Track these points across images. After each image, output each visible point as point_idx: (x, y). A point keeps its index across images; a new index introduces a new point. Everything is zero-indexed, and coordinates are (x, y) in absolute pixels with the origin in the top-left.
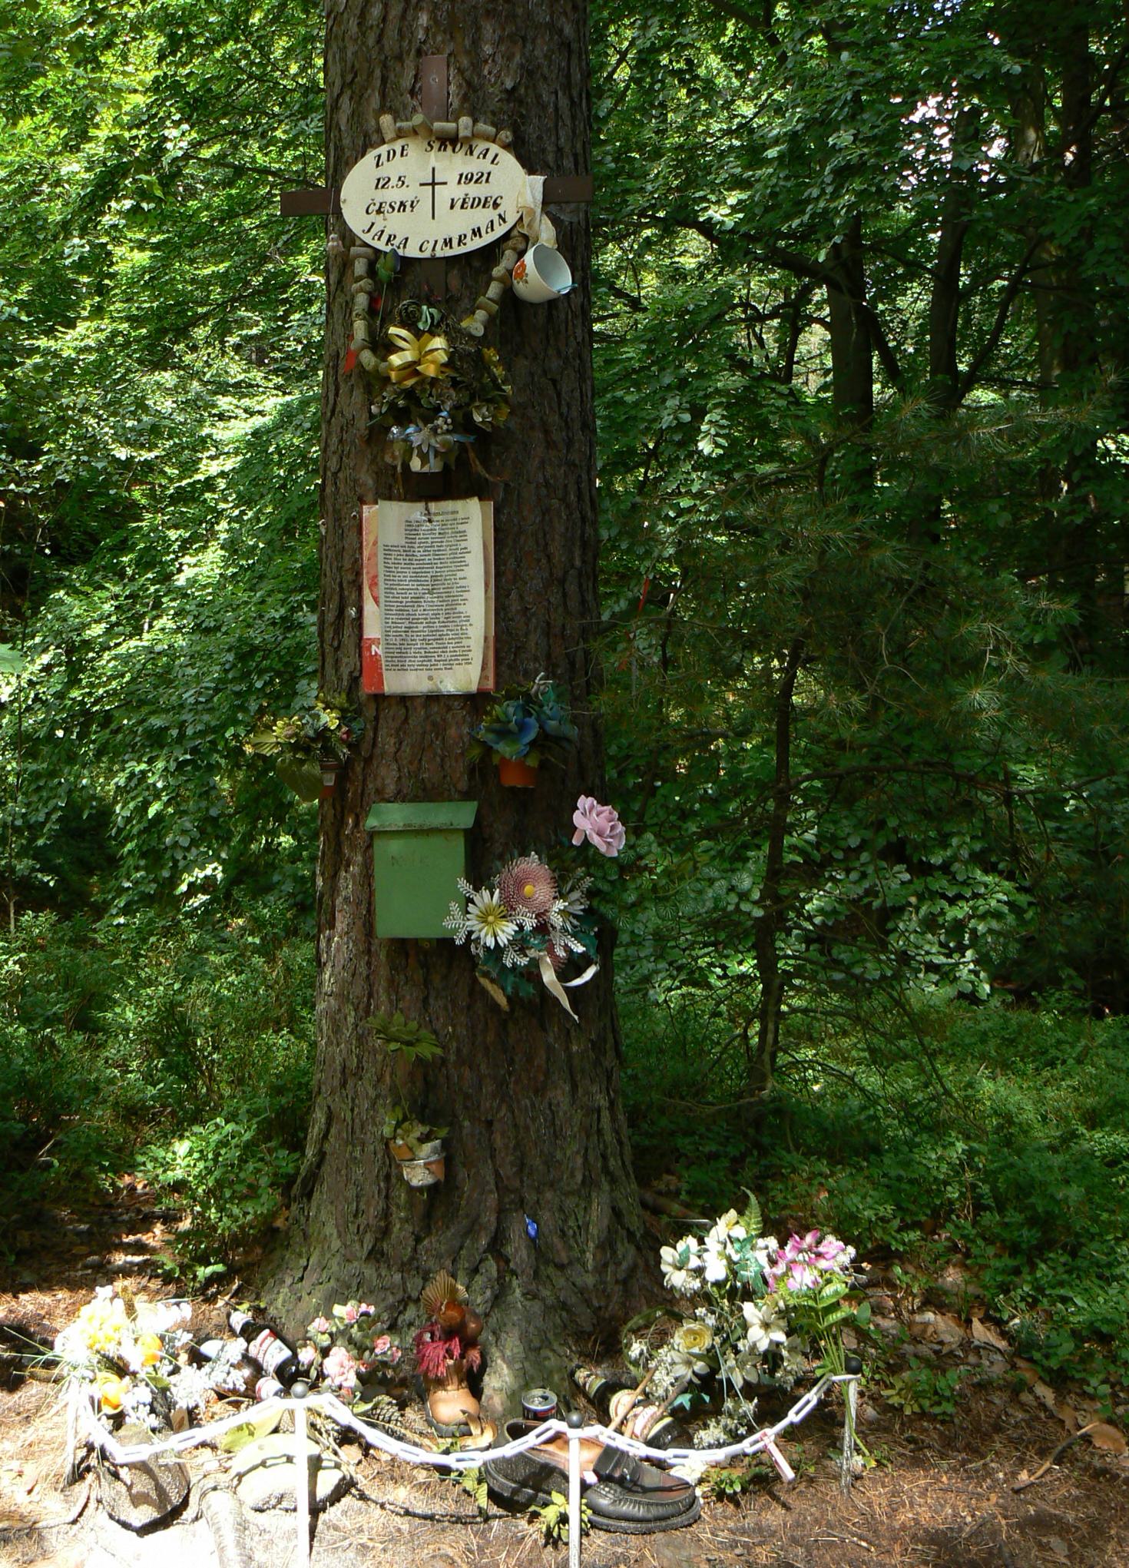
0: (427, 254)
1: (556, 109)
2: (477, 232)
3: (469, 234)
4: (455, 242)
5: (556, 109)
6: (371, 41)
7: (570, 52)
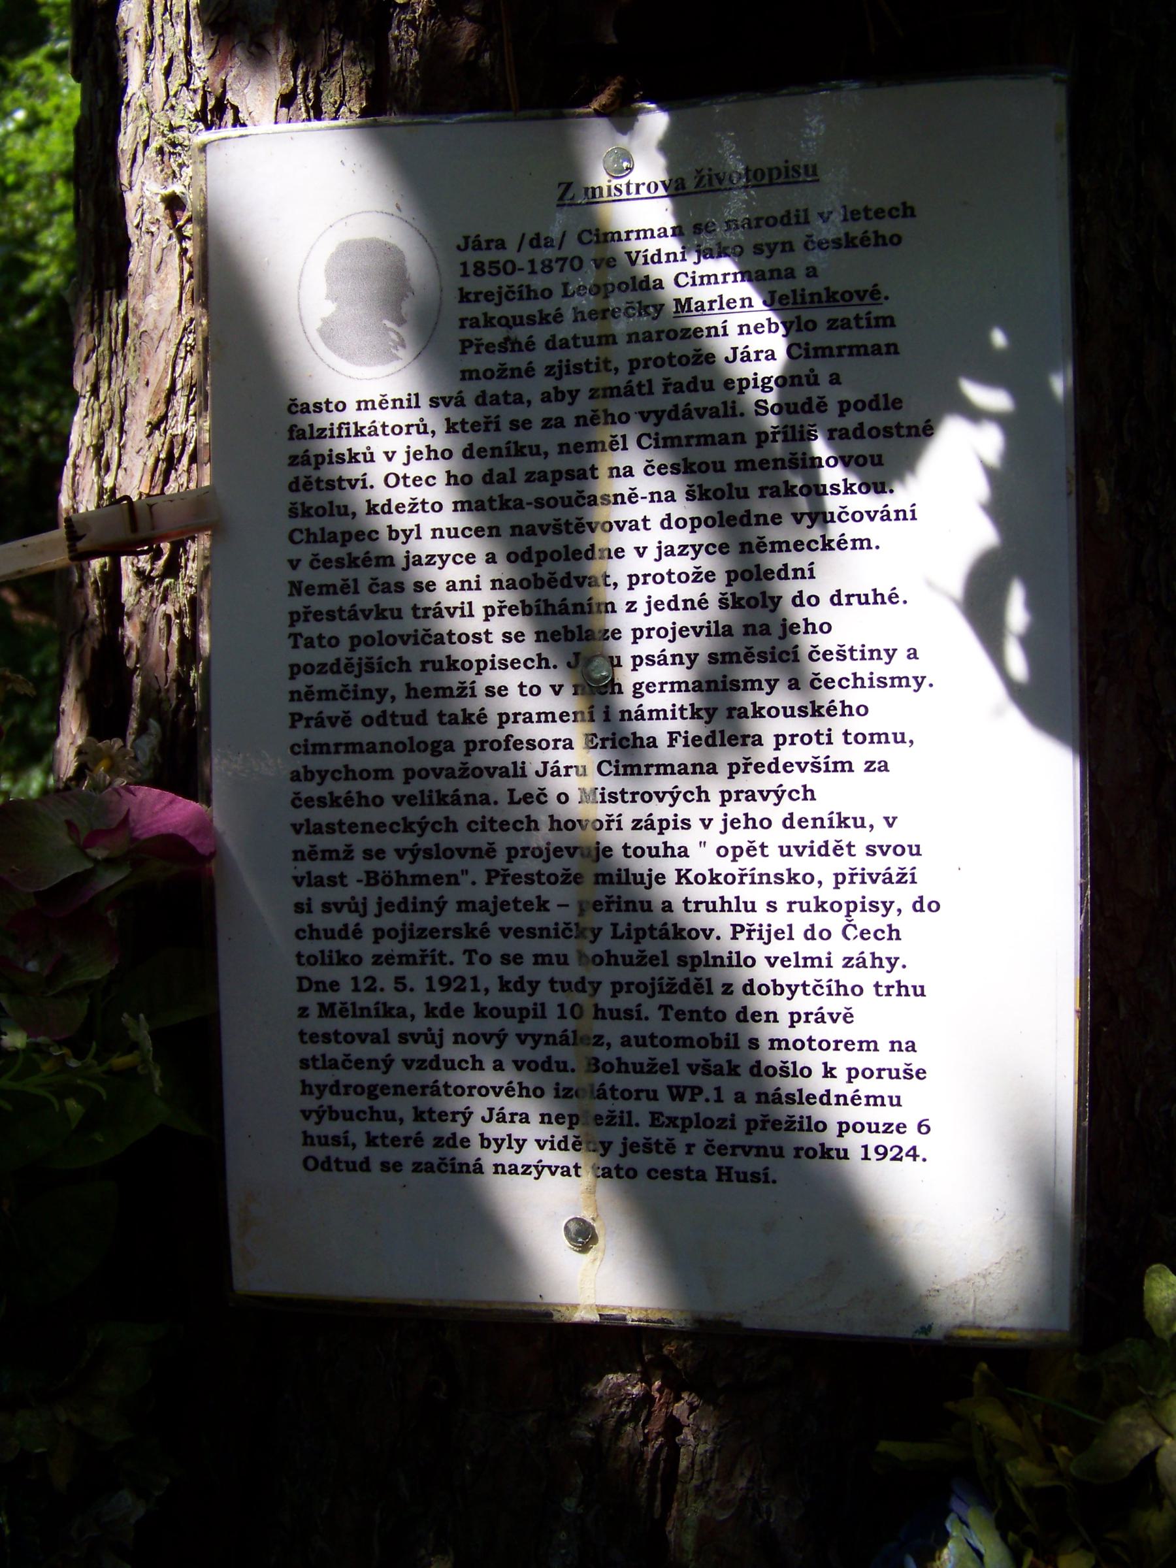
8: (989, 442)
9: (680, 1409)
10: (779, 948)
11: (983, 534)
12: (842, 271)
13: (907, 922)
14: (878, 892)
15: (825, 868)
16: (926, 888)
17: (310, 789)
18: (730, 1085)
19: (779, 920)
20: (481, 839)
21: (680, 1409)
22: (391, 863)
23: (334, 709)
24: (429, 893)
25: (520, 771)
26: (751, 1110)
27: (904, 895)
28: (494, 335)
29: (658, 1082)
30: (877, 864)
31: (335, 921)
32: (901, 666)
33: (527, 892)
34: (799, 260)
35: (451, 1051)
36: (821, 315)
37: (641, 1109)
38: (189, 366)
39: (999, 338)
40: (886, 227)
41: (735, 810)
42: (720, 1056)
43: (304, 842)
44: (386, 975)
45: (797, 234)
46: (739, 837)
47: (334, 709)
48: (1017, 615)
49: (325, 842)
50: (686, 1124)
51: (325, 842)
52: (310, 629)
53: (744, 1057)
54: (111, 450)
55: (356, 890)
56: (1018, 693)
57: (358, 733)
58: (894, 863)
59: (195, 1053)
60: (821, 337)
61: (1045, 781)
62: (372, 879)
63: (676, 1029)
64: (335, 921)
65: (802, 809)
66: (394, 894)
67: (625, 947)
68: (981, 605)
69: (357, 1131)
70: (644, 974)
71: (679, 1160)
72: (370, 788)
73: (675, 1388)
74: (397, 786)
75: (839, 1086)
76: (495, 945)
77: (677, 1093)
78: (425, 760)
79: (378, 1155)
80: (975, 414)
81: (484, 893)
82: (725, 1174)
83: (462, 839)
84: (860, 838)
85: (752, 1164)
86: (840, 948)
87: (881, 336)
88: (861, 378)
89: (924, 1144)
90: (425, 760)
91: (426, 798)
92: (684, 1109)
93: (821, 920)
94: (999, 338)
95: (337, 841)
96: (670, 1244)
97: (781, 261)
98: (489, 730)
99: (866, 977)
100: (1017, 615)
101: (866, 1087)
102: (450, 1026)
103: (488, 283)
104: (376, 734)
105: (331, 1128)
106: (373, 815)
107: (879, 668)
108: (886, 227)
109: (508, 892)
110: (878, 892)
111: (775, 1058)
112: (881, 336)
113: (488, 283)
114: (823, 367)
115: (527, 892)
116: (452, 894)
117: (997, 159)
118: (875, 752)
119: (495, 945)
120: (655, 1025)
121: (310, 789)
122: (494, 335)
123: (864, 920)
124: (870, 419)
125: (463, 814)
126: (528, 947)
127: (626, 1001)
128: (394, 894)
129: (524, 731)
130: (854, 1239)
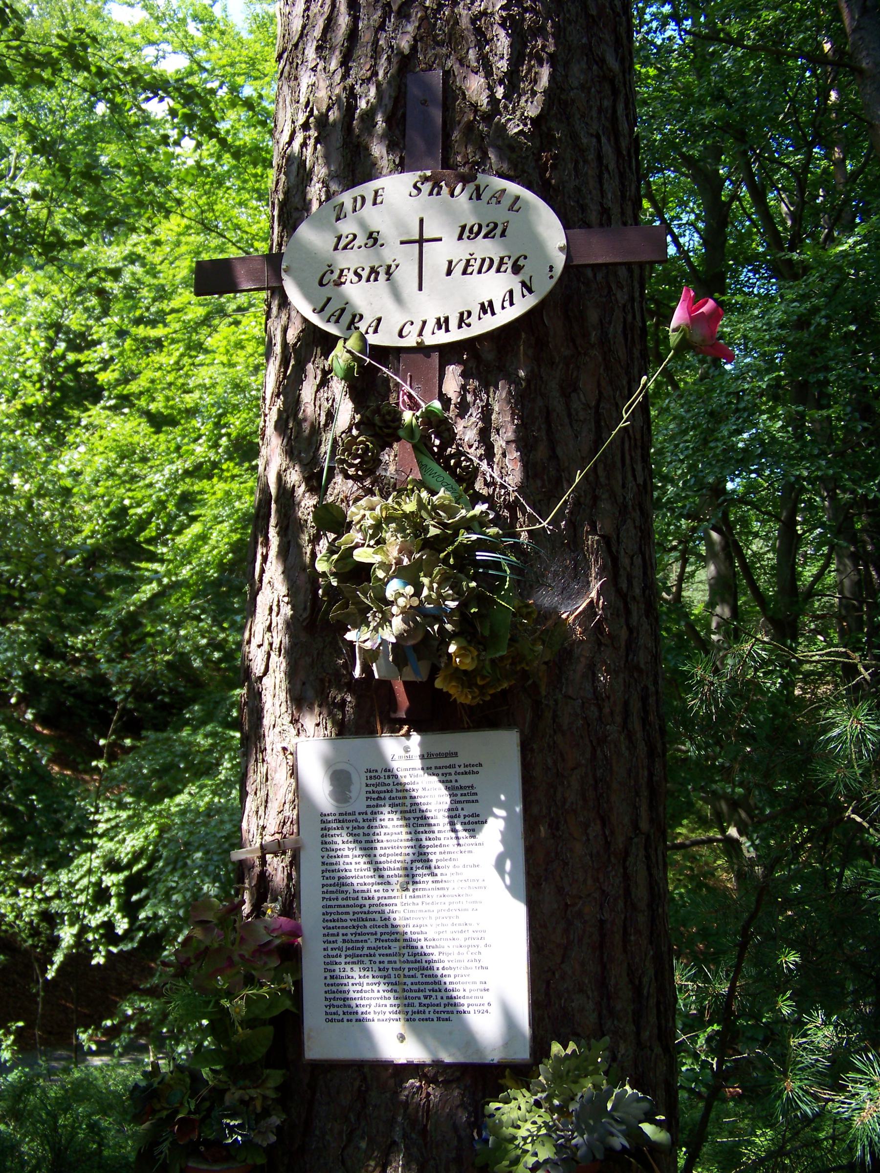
0: (410, 341)
1: (600, 158)
2: (487, 308)
3: (475, 311)
4: (453, 323)
5: (600, 158)
6: (334, 64)
7: (615, 92)
8: (500, 824)
9: (430, 1090)
10: (450, 958)
11: (500, 848)
12: (464, 781)
13: (482, 949)
14: (476, 942)
15: (462, 936)
16: (486, 941)
17: (328, 917)
18: (439, 994)
19: (450, 950)
20: (373, 930)
21: (430, 1090)
22: (349, 937)
23: (334, 896)
24: (360, 945)
25: (383, 912)
26: (445, 1001)
27: (482, 943)
28: (375, 796)
29: (421, 994)
30: (475, 935)
31: (334, 953)
32: (481, 884)
33: (385, 944)
34: (453, 778)
35: (366, 988)
36: (459, 792)
37: (416, 1002)
38: (290, 796)
39: (503, 797)
40: (475, 769)
41: (439, 921)
42: (436, 987)
43: (326, 931)
44: (348, 967)
45: (452, 771)
46: (441, 929)
47: (334, 896)
48: (508, 865)
49: (331, 931)
50: (428, 1006)
51: (331, 931)
52: (327, 874)
53: (443, 987)
54: (261, 812)
55: (340, 944)
56: (509, 888)
57: (340, 902)
58: (479, 935)
59: (297, 997)
60: (459, 798)
61: (516, 913)
62: (344, 941)
63: (425, 980)
64: (334, 953)
65: (456, 921)
66: (350, 945)
67: (412, 958)
68: (499, 866)
69: (340, 1011)
70: (417, 965)
71: (427, 1016)
72: (344, 917)
73: (428, 1083)
74: (351, 916)
75: (467, 994)
76: (377, 959)
77: (426, 997)
78: (358, 909)
79: (346, 1017)
80: (496, 817)
81: (374, 945)
82: (439, 1019)
83: (369, 930)
84: (471, 928)
85: (446, 1016)
86: (466, 957)
87: (474, 798)
88: (469, 809)
89: (490, 1009)
90: (358, 909)
91: (358, 920)
92: (427, 1001)
93: (462, 950)
94: (503, 797)
95: (335, 931)
96: (379, 754)
97: (448, 778)
98: (375, 901)
99: (474, 964)
100: (508, 865)
101: (473, 994)
102: (366, 981)
103: (373, 782)
104: (345, 903)
105: (333, 1010)
106: (344, 924)
107: (475, 884)
108: (475, 769)
109: (381, 944)
110: (476, 942)
111: (450, 987)
112: (474, 798)
113: (373, 782)
114: (459, 806)
115: (385, 944)
116: (366, 945)
117: (499, 752)
118: (475, 906)
119: (377, 959)
120: (420, 979)
121: (328, 917)
122: (375, 796)
123: (472, 950)
124: (472, 819)
125: (368, 924)
126: (386, 959)
127: (412, 973)
128: (350, 945)
129: (383, 901)
130: (468, 1038)
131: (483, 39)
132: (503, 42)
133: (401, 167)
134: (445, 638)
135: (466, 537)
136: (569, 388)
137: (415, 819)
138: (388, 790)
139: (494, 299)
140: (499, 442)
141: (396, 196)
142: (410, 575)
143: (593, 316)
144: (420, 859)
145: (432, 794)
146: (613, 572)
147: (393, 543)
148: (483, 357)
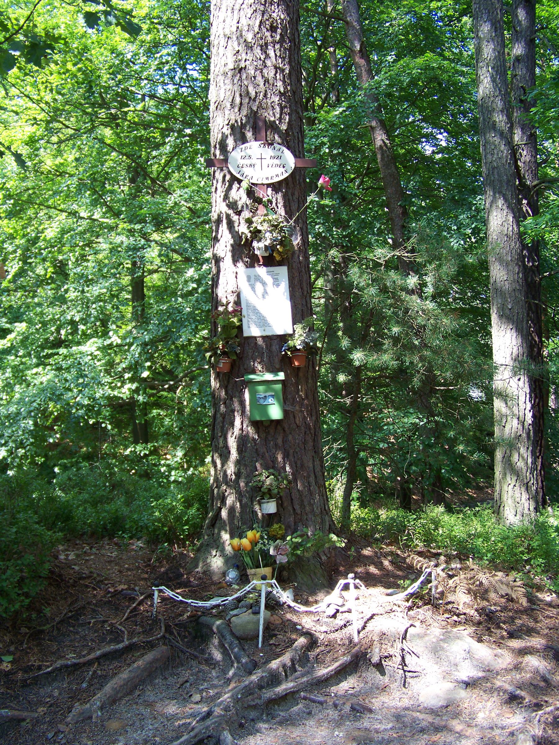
2: (277, 176)
117: (283, 271)
131: (273, 109)
132: (278, 109)
133: (256, 140)
134: (277, 245)
135: (281, 225)
136: (293, 194)
137: (264, 284)
138: (258, 278)
139: (278, 174)
140: (279, 206)
141: (254, 147)
142: (271, 232)
143: (298, 177)
144: (265, 293)
145: (268, 279)
146: (302, 235)
147: (266, 225)
148: (276, 187)
